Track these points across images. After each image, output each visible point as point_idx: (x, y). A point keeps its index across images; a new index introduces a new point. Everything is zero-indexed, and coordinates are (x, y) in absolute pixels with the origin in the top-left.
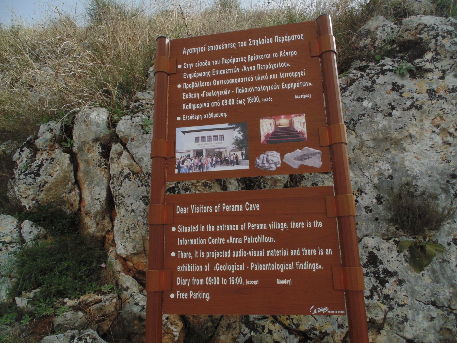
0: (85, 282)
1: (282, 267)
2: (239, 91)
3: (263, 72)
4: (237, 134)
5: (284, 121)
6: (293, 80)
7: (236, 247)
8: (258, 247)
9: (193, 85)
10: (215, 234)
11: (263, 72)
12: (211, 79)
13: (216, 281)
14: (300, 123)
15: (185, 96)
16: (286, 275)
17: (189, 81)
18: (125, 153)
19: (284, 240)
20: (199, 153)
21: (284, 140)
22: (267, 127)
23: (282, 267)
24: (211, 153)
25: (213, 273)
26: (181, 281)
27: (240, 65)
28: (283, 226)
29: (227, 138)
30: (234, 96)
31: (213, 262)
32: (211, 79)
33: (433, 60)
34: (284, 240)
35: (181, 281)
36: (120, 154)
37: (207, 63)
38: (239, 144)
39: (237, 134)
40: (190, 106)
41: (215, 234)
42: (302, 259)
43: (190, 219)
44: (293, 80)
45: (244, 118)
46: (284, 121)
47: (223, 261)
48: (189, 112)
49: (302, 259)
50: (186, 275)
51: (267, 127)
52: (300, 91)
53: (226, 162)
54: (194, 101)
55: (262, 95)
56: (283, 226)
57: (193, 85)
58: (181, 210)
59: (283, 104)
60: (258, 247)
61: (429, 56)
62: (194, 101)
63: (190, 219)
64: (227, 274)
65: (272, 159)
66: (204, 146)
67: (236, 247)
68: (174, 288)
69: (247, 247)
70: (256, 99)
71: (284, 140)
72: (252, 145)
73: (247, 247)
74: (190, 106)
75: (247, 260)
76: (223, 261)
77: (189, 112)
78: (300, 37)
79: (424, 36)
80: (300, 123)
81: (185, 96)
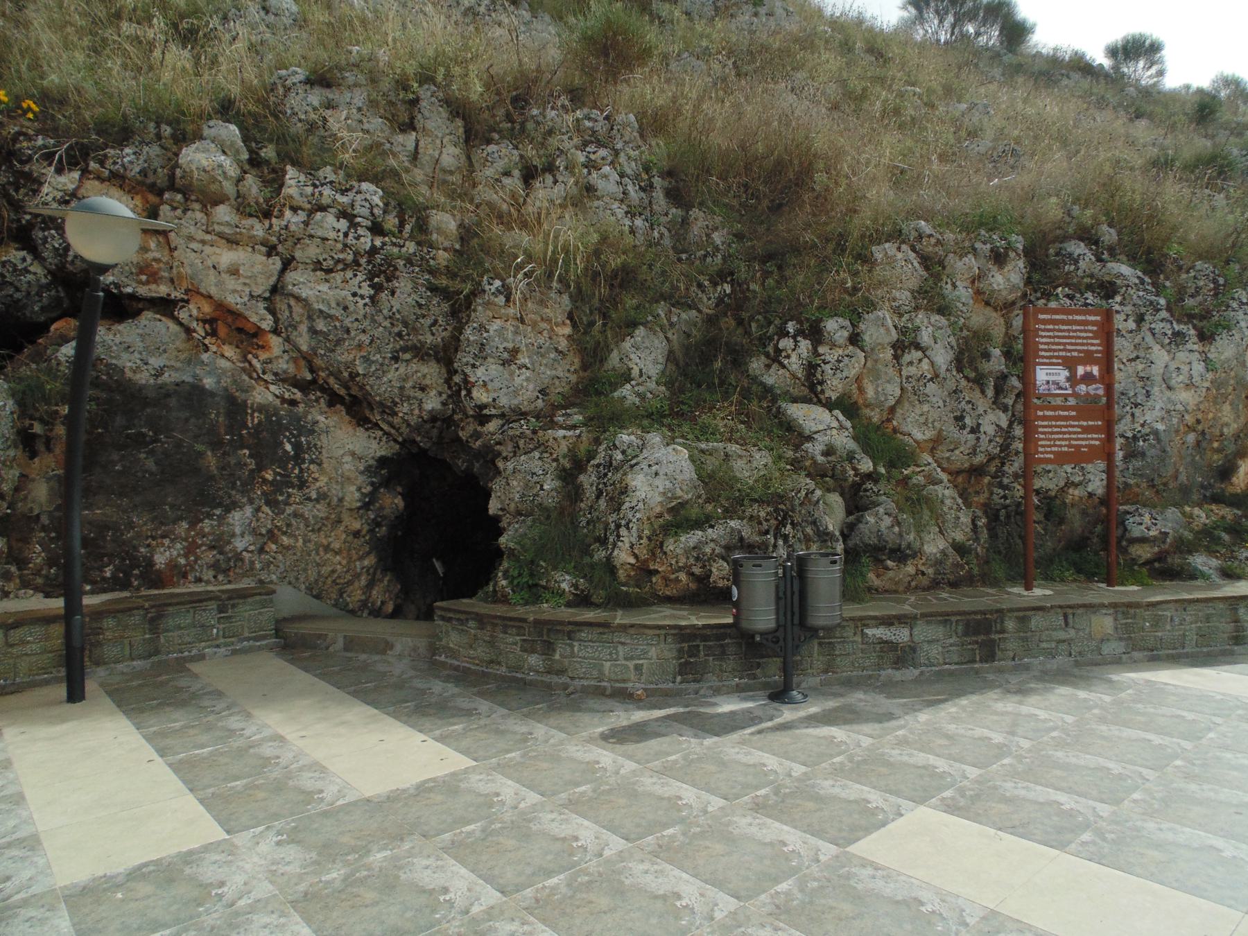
0: (279, 529)
1: (1084, 443)
2: (1068, 347)
3: (1079, 338)
4: (1066, 373)
5: (1088, 368)
6: (1092, 345)
7: (1064, 433)
8: (1075, 433)
9: (1044, 340)
10: (1056, 426)
11: (1079, 338)
12: (1054, 337)
13: (1055, 449)
14: (1095, 370)
15: (1041, 347)
16: (1085, 446)
17: (1042, 337)
18: (926, 360)
19: (1086, 430)
20: (1048, 382)
21: (1088, 378)
22: (1081, 370)
23: (1084, 443)
24: (1054, 383)
25: (1055, 446)
26: (1040, 449)
27: (1068, 331)
28: (1085, 424)
29: (1062, 375)
30: (1065, 350)
31: (1055, 440)
32: (1054, 337)
33: (1121, 304)
34: (1086, 430)
35: (1040, 449)
36: (920, 360)
37: (1051, 327)
38: (1068, 379)
39: (1066, 373)
40: (1043, 353)
41: (1056, 426)
42: (1092, 439)
43: (1044, 418)
44: (1092, 345)
45: (1070, 364)
46: (1088, 368)
47: (1059, 439)
48: (1043, 357)
49: (1092, 439)
50: (1043, 446)
51: (1081, 370)
52: (1097, 352)
53: (1061, 388)
54: (1045, 350)
55: (1079, 351)
56: (1085, 424)
57: (1044, 340)
58: (1040, 413)
59: (1088, 358)
60: (1075, 433)
61: (1118, 298)
62: (1045, 350)
63: (1044, 418)
64: (1061, 446)
65: (1082, 388)
66: (1051, 378)
67: (1064, 433)
68: (1038, 452)
69: (1070, 433)
70: (1075, 354)
71: (1088, 378)
72: (1072, 380)
73: (1070, 433)
74: (1043, 353)
75: (1070, 439)
76: (1059, 439)
77: (1043, 357)
78: (1098, 318)
79: (1118, 282)
80: (1095, 370)
81: (1041, 347)
